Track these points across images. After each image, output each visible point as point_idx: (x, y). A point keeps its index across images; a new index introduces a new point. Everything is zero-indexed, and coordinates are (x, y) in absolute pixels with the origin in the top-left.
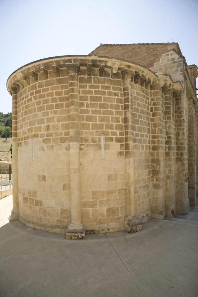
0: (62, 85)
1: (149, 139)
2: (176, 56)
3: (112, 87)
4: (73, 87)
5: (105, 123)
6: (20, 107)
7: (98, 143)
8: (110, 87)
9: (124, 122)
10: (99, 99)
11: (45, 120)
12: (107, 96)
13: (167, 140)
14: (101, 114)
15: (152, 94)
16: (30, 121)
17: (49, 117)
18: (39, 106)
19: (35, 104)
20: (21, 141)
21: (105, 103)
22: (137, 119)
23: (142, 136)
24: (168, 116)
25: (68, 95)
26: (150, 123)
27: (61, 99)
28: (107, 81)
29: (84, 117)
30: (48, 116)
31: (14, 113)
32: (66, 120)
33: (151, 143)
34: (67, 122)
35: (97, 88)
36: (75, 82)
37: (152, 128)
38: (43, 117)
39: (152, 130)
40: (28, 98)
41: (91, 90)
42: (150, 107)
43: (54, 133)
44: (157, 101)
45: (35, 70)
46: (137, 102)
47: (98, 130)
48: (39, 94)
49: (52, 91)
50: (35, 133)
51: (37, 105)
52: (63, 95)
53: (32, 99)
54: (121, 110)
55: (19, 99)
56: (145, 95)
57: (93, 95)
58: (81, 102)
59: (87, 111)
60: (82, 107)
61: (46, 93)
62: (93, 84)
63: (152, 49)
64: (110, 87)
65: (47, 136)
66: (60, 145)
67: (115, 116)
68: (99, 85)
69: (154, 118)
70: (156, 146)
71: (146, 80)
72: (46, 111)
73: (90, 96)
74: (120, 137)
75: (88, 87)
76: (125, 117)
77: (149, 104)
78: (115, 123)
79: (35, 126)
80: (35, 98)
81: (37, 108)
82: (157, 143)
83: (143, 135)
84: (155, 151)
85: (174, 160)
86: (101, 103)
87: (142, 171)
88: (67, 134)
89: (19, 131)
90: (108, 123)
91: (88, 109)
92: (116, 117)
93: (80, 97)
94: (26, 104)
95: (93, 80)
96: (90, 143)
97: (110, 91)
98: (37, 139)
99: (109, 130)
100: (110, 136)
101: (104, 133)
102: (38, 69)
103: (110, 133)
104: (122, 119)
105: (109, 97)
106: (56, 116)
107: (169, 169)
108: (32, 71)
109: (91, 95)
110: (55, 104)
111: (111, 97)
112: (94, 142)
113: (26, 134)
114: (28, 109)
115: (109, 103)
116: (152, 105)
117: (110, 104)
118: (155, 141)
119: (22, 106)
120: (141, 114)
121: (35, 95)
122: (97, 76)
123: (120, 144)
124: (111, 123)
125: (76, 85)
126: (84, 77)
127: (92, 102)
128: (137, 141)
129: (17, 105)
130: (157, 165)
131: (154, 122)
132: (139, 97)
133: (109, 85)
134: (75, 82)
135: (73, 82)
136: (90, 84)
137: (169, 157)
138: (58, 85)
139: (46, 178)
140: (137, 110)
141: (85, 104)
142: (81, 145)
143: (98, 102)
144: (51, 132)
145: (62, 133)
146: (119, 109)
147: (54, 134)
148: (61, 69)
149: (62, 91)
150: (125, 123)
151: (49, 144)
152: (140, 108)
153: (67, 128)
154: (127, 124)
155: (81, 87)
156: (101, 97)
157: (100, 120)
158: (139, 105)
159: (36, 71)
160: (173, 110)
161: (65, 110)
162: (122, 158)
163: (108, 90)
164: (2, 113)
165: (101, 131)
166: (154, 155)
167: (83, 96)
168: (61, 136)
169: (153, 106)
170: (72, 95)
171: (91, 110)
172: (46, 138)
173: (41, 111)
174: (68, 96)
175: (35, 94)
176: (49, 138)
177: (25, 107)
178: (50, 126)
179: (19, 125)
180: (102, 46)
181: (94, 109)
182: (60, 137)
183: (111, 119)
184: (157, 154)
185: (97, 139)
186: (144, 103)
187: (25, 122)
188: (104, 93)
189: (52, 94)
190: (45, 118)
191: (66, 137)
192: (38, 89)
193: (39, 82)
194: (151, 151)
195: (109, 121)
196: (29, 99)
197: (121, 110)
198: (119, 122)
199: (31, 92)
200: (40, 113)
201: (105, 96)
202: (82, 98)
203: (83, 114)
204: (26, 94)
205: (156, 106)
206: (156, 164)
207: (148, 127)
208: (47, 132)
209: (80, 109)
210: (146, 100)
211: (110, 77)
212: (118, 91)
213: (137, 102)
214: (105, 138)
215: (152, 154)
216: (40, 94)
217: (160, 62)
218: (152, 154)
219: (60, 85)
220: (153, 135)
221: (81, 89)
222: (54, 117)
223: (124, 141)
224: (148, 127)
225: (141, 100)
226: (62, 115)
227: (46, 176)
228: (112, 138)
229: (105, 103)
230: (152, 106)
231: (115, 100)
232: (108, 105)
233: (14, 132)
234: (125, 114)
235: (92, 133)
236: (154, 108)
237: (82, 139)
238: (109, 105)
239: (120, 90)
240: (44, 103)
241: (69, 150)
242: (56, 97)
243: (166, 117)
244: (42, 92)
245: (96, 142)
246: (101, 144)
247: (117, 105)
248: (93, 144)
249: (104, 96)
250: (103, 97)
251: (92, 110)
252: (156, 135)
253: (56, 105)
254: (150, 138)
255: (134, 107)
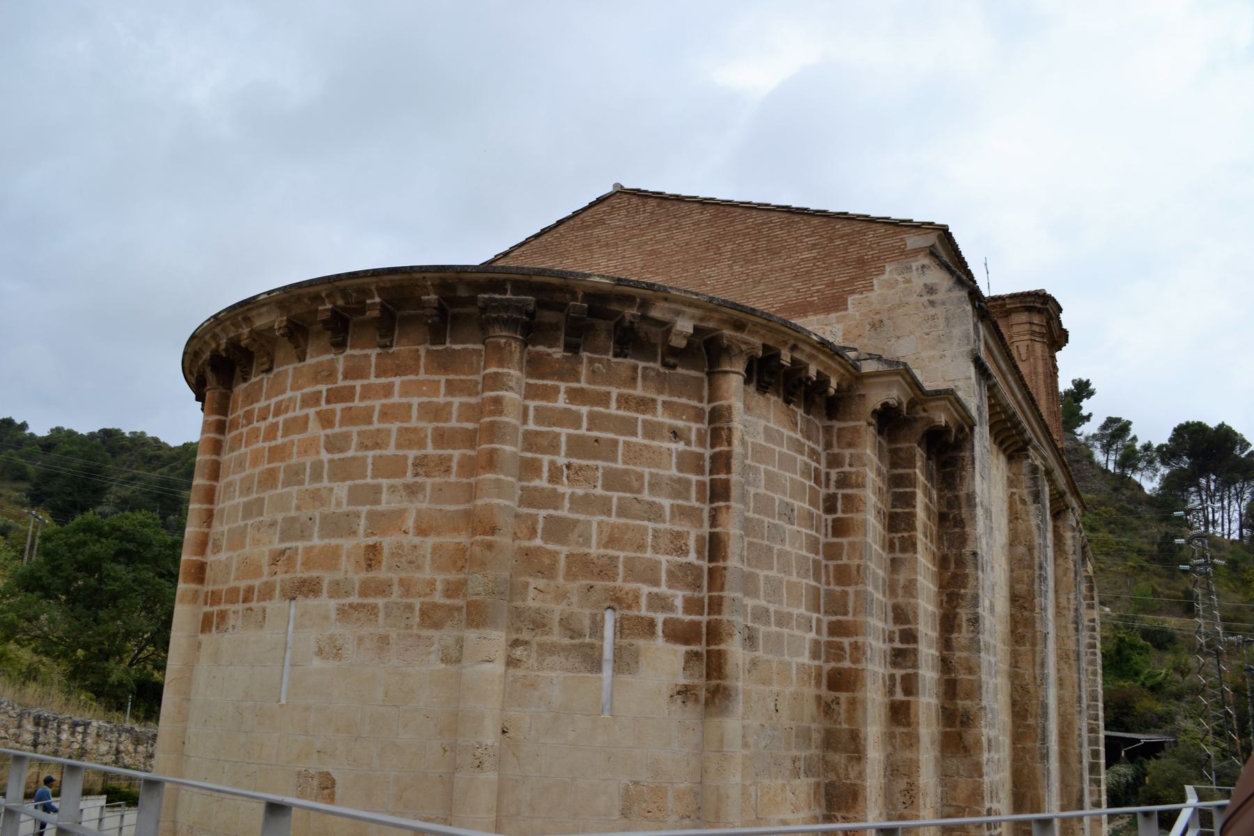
0: (451, 377)
1: (813, 635)
2: (938, 277)
3: (664, 402)
4: (500, 393)
5: (626, 553)
6: (243, 450)
7: (587, 640)
8: (654, 401)
9: (707, 554)
10: (607, 450)
11: (363, 522)
12: (639, 439)
13: (898, 645)
14: (610, 515)
15: (835, 439)
16: (285, 520)
17: (382, 507)
18: (337, 456)
19: (322, 444)
20: (223, 607)
21: (631, 467)
22: (766, 542)
23: (783, 620)
24: (906, 534)
25: (477, 421)
26: (824, 562)
27: (442, 438)
28: (645, 378)
29: (535, 522)
30: (377, 502)
31: (206, 471)
32: (456, 530)
33: (823, 658)
34: (463, 539)
35: (598, 404)
36: (512, 372)
37: (832, 587)
38: (351, 508)
39: (829, 594)
40: (290, 415)
41: (574, 407)
42: (823, 491)
43: (396, 581)
44: (853, 470)
45: (340, 302)
46: (766, 472)
47: (592, 583)
48: (344, 405)
49: (404, 400)
50: (306, 575)
51: (328, 450)
52: (454, 420)
53: (306, 423)
54: (694, 503)
55: (240, 412)
56: (803, 440)
57: (583, 431)
58: (529, 455)
59: (553, 499)
60: (529, 480)
61: (377, 404)
62: (583, 384)
63: (841, 237)
64: (654, 401)
65: (363, 594)
66: (419, 637)
67: (668, 526)
68: (609, 393)
69: (840, 545)
70: (845, 670)
71: (809, 378)
72: (369, 480)
73: (569, 436)
74: (688, 618)
75: (562, 396)
76: (711, 534)
77: (817, 481)
78: (669, 558)
79: (308, 544)
80: (326, 420)
81: (326, 466)
82: (851, 655)
83: (790, 615)
84: (843, 696)
85: (933, 743)
86: (611, 468)
87: (780, 781)
88: (453, 590)
89: (223, 556)
90: (639, 555)
91: (555, 490)
92: (671, 532)
93: (527, 434)
94: (275, 438)
95: (584, 371)
96: (556, 637)
97: (655, 419)
98: (312, 602)
99: (639, 585)
100: (644, 612)
101: (617, 601)
102: (357, 303)
103: (643, 601)
104: (700, 539)
105: (647, 442)
106: (414, 509)
107: (904, 786)
108: (329, 306)
109: (571, 431)
110: (412, 454)
111: (655, 443)
112: (574, 633)
113: (257, 573)
114: (282, 465)
115: (647, 471)
116: (832, 483)
117: (651, 474)
118: (840, 647)
119: (255, 447)
120: (780, 523)
121: (324, 406)
122: (606, 353)
123: (683, 649)
124: (649, 554)
125: (512, 384)
126: (549, 355)
127: (574, 461)
128: (761, 642)
129: (221, 437)
130: (850, 759)
131: (840, 562)
132: (777, 449)
133: (650, 395)
134: (509, 375)
135: (500, 370)
136: (574, 385)
137: (909, 724)
138: (436, 377)
139: (339, 790)
140: (764, 505)
141: (545, 469)
142: (515, 643)
143: (600, 463)
144: (382, 574)
145: (432, 584)
146: (687, 499)
147: (395, 588)
148: (456, 310)
149: (450, 404)
150: (710, 561)
151: (367, 630)
152: (777, 497)
153: (460, 564)
154: (721, 564)
155: (532, 392)
156: (615, 443)
157: (605, 540)
158: (771, 481)
159: (343, 309)
160: (927, 508)
161: (457, 483)
162: (688, 715)
163: (644, 412)
164: (24, 426)
165: (606, 590)
166: (839, 713)
167: (537, 433)
168: (426, 595)
169: (838, 488)
170: (492, 424)
171: (567, 496)
172: (355, 599)
173: (343, 480)
174: (477, 426)
175: (328, 402)
176: (371, 600)
177: (267, 454)
178: (382, 549)
179: (220, 528)
180: (620, 193)
181: (580, 492)
182: (422, 603)
183: (650, 537)
184: (848, 711)
185: (587, 622)
186: (798, 477)
187: (261, 522)
188: (628, 427)
189: (400, 412)
190: (364, 509)
191: (448, 602)
192: (341, 383)
193: (349, 352)
194: (824, 691)
195: (641, 547)
196: (295, 419)
197: (694, 503)
198: (687, 553)
199: (306, 390)
200: (341, 490)
201: (633, 439)
202: (531, 441)
203: (534, 507)
204: (280, 398)
205: (849, 491)
206: (844, 756)
207: (813, 583)
208: (364, 575)
209: (522, 489)
210: (806, 464)
211: (655, 361)
212: (688, 420)
213: (766, 472)
214: (622, 618)
215: (828, 705)
216: (350, 404)
217: (873, 296)
218: (828, 705)
219: (443, 378)
220: (834, 618)
221: (532, 404)
222: (401, 514)
223: (704, 638)
224: (813, 583)
225: (786, 463)
226: (438, 507)
227: (335, 775)
228: (652, 624)
229: (631, 467)
230: (832, 490)
231: (674, 460)
232: (640, 477)
233: (194, 558)
234: (714, 521)
235: (562, 596)
236: (839, 496)
237: (519, 617)
238: (647, 478)
239: (698, 416)
240: (363, 446)
241: (458, 661)
242: (422, 424)
243: (896, 541)
244: (363, 398)
245: (581, 635)
246: (602, 646)
247: (679, 481)
248: (566, 641)
249: (627, 438)
250: (625, 442)
251: (573, 493)
252: (848, 622)
253: (416, 458)
254: (819, 632)
255: (752, 490)
